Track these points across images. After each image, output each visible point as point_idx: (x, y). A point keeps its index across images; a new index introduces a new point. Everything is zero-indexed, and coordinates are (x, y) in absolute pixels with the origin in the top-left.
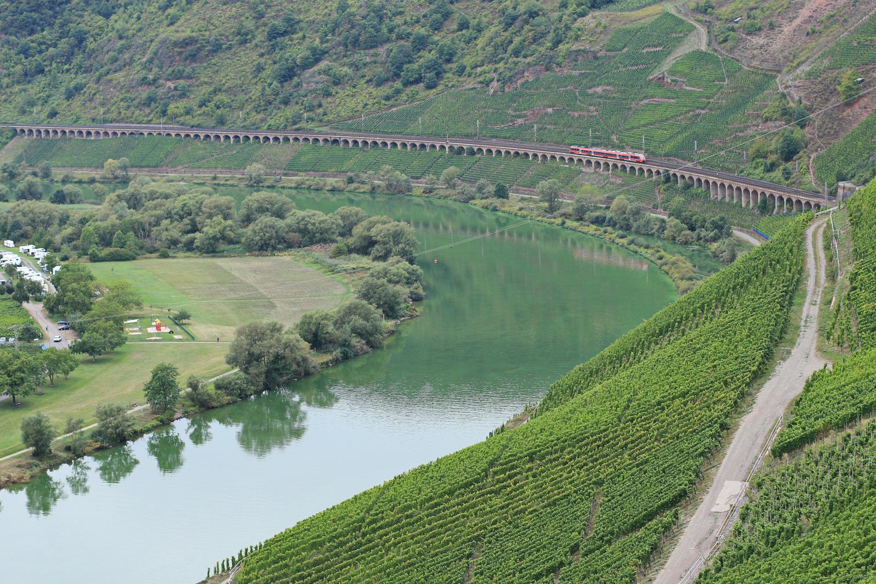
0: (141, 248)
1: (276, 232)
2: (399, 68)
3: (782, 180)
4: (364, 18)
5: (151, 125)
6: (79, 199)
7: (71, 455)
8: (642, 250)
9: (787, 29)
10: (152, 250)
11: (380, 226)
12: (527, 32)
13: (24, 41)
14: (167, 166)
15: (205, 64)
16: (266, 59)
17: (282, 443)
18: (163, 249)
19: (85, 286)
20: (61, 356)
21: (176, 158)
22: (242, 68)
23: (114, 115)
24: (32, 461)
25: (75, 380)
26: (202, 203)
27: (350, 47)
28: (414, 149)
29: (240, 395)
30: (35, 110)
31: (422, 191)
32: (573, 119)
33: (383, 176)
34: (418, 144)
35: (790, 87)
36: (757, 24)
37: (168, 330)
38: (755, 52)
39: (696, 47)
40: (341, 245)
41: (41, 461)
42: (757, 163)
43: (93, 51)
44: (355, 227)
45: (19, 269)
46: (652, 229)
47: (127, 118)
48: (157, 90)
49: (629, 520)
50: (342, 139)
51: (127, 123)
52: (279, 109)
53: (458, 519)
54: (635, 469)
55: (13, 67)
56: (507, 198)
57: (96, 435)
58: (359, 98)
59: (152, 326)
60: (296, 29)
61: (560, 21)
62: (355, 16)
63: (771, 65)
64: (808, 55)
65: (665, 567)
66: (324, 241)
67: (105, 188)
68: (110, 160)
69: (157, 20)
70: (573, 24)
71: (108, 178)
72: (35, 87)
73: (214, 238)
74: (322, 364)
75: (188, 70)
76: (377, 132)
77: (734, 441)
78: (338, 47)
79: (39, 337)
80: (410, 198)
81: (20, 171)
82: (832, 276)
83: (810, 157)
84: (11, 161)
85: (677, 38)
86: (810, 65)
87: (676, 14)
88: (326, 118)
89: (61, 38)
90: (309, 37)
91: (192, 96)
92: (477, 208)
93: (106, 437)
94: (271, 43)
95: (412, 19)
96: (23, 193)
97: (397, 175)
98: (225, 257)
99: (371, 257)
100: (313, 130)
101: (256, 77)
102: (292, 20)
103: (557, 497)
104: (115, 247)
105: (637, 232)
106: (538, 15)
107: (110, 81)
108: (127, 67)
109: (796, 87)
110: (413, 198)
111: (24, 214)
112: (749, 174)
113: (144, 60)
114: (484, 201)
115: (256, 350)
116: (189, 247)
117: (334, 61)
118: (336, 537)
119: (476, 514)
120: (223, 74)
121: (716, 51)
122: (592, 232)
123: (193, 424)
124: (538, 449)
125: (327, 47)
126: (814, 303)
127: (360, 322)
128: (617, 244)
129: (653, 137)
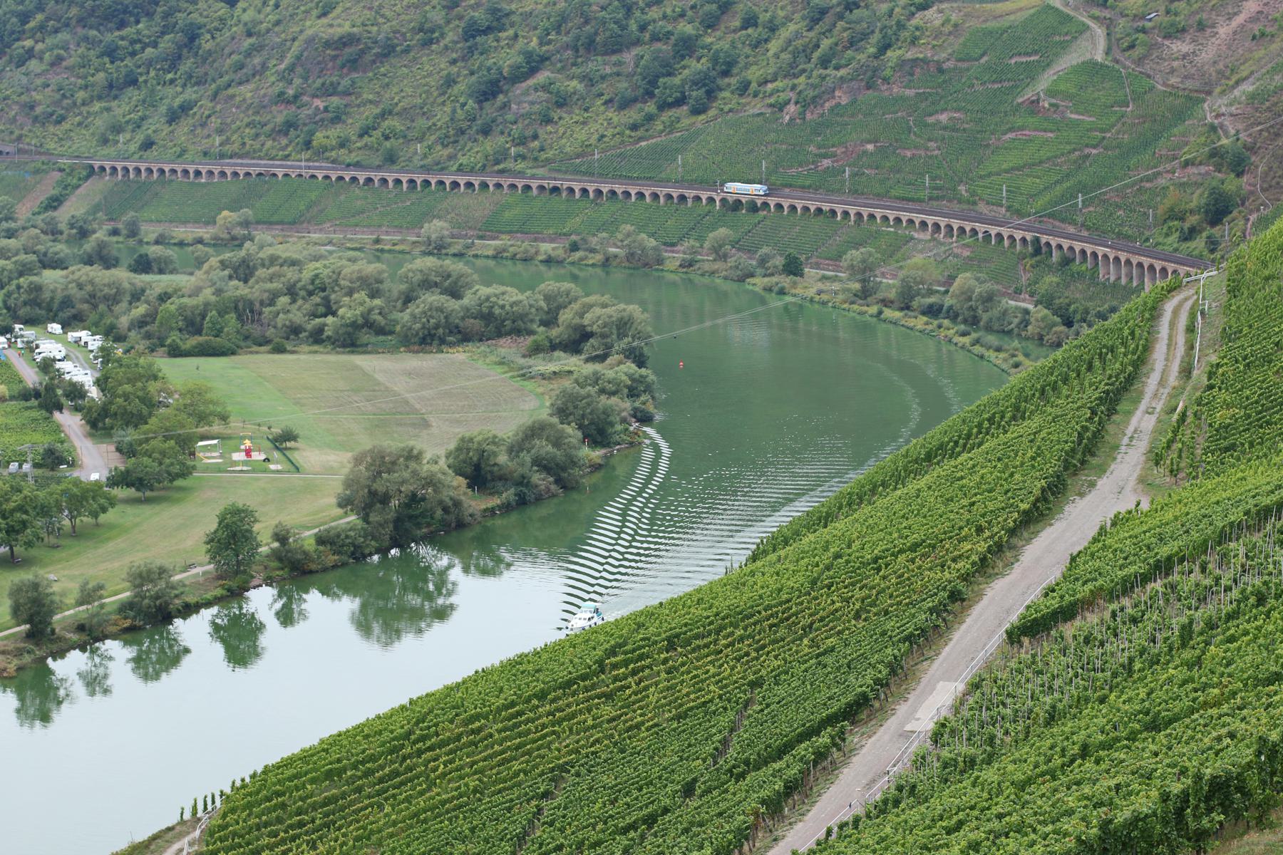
0: (246, 338)
1: (446, 317)
2: (653, 83)
3: (1205, 253)
4: (603, 8)
5: (289, 163)
6: (171, 267)
7: (84, 637)
8: (991, 354)
9: (1224, 31)
10: (261, 342)
11: (598, 311)
12: (841, 31)
13: (109, 37)
14: (309, 222)
15: (370, 74)
16: (460, 68)
17: (420, 631)
18: (277, 340)
19: (144, 388)
20: (88, 491)
21: (322, 211)
22: (423, 81)
23: (235, 147)
24: (22, 645)
25: (111, 527)
26: (339, 273)
27: (582, 51)
28: (669, 202)
29: (353, 553)
30: (121, 138)
31: (678, 263)
32: (903, 160)
33: (622, 241)
34: (675, 195)
35: (1223, 115)
36: (1179, 23)
37: (263, 457)
38: (1175, 64)
39: (1088, 57)
40: (540, 339)
41: (37, 645)
42: (1169, 228)
43: (210, 53)
44: (561, 312)
45: (58, 365)
46: (1010, 323)
47: (255, 151)
48: (299, 112)
49: (776, 741)
50: (565, 187)
51: (254, 158)
52: (475, 140)
53: (544, 737)
54: (813, 661)
55: (93, 75)
56: (802, 275)
57: (125, 608)
58: (593, 127)
59: (239, 450)
60: (504, 25)
61: (890, 16)
62: (590, 5)
63: (1197, 84)
64: (1252, 69)
65: (806, 818)
66: (518, 332)
67: (210, 250)
68: (225, 213)
69: (303, 8)
70: (909, 20)
71: (222, 239)
72: (124, 105)
73: (354, 325)
74: (485, 510)
75: (345, 82)
76: (630, 180)
77: (969, 620)
78: (565, 51)
79: (68, 463)
80: (660, 274)
81: (96, 226)
82: (1186, 372)
83: (1248, 220)
84: (82, 211)
85: (1061, 43)
86: (1254, 84)
87: (1061, 8)
88: (543, 156)
89: (163, 33)
90: (523, 37)
91: (350, 121)
92: (757, 289)
93: (139, 612)
94: (468, 44)
95: (674, 11)
96: (90, 257)
97: (643, 240)
98: (369, 353)
99: (583, 357)
100: (524, 173)
101: (444, 94)
102: (499, 10)
103: (692, 704)
104: (207, 335)
105: (989, 329)
106: (858, 7)
107: (233, 96)
108: (257, 77)
109: (1232, 115)
110: (665, 273)
111: (80, 286)
112: (1158, 244)
113: (283, 66)
114: (766, 280)
115: (379, 487)
116: (317, 337)
117: (559, 71)
118: (363, 762)
119: (571, 730)
120: (395, 90)
121: (1117, 62)
122: (919, 327)
123: (280, 596)
124: (684, 629)
125: (548, 51)
126: (1150, 410)
127: (544, 448)
128: (956, 344)
129: (1019, 188)
